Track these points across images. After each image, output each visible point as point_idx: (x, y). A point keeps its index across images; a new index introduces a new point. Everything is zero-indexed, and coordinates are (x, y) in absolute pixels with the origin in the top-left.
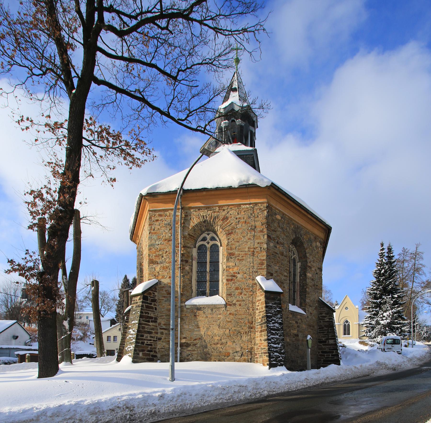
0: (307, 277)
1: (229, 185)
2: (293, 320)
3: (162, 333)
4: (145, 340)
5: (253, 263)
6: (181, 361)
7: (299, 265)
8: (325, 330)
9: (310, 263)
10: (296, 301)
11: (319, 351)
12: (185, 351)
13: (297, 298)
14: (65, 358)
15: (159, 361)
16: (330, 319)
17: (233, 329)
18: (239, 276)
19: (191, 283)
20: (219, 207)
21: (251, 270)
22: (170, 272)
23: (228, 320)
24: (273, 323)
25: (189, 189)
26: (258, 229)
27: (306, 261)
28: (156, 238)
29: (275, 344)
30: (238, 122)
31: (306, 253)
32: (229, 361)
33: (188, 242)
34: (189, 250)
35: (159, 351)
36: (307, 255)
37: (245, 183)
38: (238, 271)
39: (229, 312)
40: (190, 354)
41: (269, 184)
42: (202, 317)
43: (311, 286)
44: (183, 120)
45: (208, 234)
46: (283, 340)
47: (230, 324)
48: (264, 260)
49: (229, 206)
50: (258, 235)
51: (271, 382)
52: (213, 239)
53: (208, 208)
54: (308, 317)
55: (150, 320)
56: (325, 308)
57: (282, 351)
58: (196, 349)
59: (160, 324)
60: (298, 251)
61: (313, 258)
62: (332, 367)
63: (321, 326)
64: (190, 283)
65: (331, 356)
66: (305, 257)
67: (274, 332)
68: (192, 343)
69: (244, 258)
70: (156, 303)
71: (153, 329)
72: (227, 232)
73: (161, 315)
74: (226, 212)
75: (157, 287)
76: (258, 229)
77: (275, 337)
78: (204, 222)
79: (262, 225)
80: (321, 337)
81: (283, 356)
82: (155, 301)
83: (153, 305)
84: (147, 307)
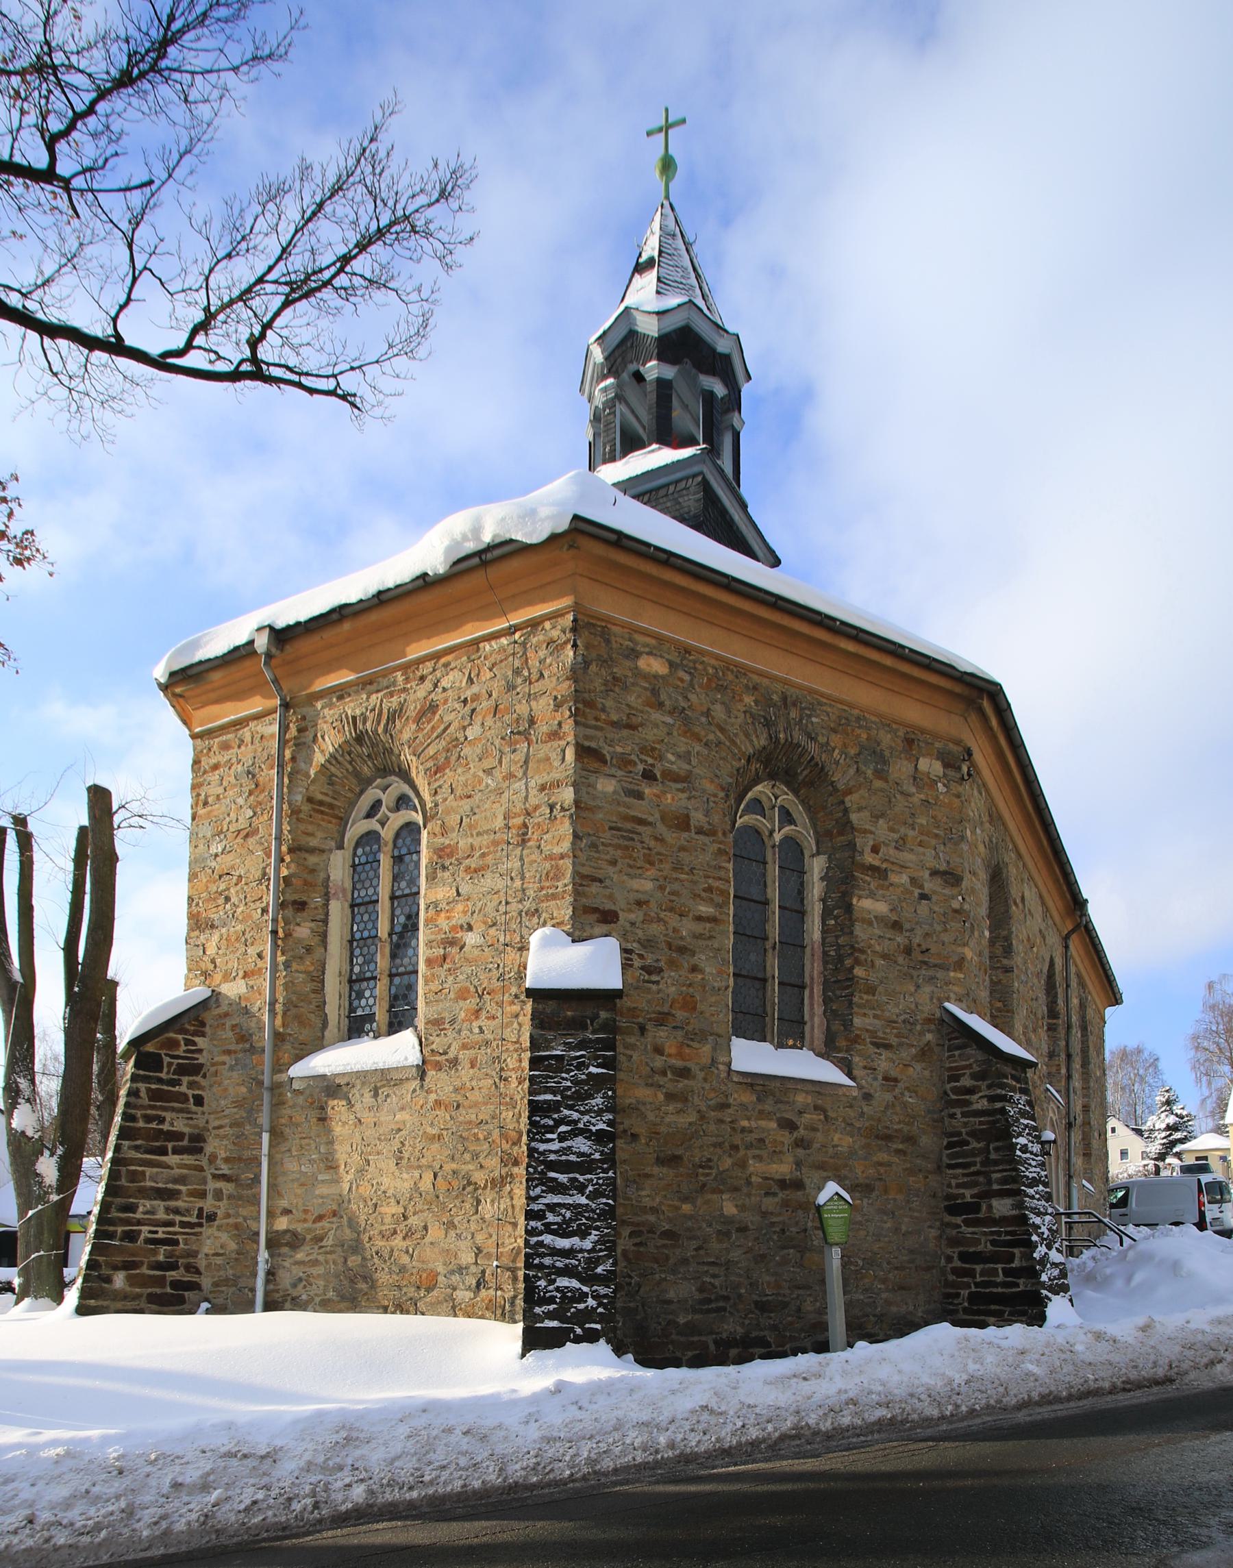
0: (856, 915)
1: (417, 571)
2: (762, 1115)
3: (218, 1195)
4: (139, 1223)
5: (523, 878)
6: (270, 1306)
7: (817, 867)
8: (973, 1153)
9: (875, 850)
10: (807, 1028)
11: (949, 1251)
12: (286, 1264)
13: (812, 1016)
14: (33, 1284)
15: (205, 1305)
16: (992, 1099)
17: (450, 1167)
18: (471, 939)
19: (320, 990)
20: (405, 668)
21: (514, 907)
22: (246, 953)
23: (429, 1130)
24: (562, 1138)
25: (291, 623)
26: (543, 728)
27: (852, 846)
28: (209, 835)
29: (565, 1235)
30: (652, 369)
31: (846, 811)
32: (434, 1309)
33: (310, 828)
34: (312, 860)
35: (208, 1266)
36: (854, 817)
37: (471, 547)
38: (467, 918)
39: (433, 1097)
40: (300, 1280)
41: (563, 525)
42: (345, 1123)
43: (884, 956)
44: (180, 353)
45: (384, 789)
46: (608, 1213)
47: (436, 1146)
48: (562, 857)
49: (436, 656)
50: (541, 755)
51: (449, 1431)
52: (402, 802)
53: (366, 684)
54: (867, 1097)
55: (170, 1145)
56: (969, 1051)
57: (599, 1270)
58: (321, 1258)
59: (213, 1159)
60: (809, 809)
61: (892, 830)
62: (1016, 1334)
63: (952, 1135)
64: (314, 991)
65: (1000, 1278)
66: (845, 826)
67: (563, 1178)
68: (309, 1230)
69: (489, 860)
70: (198, 1079)
71: (182, 1180)
72: (430, 764)
73: (217, 1123)
74: (428, 685)
75: (208, 1017)
76: (543, 728)
77: (569, 1200)
78: (359, 739)
79: (558, 706)
80: (958, 1186)
81: (603, 1291)
82: (196, 1069)
83: (183, 1089)
84: (155, 1095)
